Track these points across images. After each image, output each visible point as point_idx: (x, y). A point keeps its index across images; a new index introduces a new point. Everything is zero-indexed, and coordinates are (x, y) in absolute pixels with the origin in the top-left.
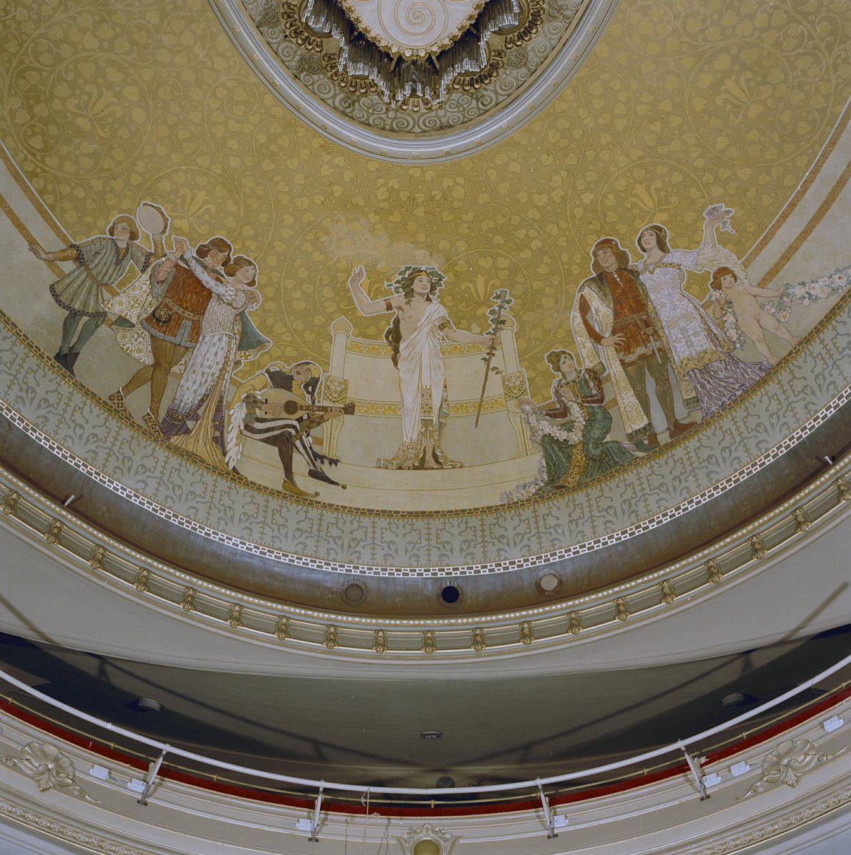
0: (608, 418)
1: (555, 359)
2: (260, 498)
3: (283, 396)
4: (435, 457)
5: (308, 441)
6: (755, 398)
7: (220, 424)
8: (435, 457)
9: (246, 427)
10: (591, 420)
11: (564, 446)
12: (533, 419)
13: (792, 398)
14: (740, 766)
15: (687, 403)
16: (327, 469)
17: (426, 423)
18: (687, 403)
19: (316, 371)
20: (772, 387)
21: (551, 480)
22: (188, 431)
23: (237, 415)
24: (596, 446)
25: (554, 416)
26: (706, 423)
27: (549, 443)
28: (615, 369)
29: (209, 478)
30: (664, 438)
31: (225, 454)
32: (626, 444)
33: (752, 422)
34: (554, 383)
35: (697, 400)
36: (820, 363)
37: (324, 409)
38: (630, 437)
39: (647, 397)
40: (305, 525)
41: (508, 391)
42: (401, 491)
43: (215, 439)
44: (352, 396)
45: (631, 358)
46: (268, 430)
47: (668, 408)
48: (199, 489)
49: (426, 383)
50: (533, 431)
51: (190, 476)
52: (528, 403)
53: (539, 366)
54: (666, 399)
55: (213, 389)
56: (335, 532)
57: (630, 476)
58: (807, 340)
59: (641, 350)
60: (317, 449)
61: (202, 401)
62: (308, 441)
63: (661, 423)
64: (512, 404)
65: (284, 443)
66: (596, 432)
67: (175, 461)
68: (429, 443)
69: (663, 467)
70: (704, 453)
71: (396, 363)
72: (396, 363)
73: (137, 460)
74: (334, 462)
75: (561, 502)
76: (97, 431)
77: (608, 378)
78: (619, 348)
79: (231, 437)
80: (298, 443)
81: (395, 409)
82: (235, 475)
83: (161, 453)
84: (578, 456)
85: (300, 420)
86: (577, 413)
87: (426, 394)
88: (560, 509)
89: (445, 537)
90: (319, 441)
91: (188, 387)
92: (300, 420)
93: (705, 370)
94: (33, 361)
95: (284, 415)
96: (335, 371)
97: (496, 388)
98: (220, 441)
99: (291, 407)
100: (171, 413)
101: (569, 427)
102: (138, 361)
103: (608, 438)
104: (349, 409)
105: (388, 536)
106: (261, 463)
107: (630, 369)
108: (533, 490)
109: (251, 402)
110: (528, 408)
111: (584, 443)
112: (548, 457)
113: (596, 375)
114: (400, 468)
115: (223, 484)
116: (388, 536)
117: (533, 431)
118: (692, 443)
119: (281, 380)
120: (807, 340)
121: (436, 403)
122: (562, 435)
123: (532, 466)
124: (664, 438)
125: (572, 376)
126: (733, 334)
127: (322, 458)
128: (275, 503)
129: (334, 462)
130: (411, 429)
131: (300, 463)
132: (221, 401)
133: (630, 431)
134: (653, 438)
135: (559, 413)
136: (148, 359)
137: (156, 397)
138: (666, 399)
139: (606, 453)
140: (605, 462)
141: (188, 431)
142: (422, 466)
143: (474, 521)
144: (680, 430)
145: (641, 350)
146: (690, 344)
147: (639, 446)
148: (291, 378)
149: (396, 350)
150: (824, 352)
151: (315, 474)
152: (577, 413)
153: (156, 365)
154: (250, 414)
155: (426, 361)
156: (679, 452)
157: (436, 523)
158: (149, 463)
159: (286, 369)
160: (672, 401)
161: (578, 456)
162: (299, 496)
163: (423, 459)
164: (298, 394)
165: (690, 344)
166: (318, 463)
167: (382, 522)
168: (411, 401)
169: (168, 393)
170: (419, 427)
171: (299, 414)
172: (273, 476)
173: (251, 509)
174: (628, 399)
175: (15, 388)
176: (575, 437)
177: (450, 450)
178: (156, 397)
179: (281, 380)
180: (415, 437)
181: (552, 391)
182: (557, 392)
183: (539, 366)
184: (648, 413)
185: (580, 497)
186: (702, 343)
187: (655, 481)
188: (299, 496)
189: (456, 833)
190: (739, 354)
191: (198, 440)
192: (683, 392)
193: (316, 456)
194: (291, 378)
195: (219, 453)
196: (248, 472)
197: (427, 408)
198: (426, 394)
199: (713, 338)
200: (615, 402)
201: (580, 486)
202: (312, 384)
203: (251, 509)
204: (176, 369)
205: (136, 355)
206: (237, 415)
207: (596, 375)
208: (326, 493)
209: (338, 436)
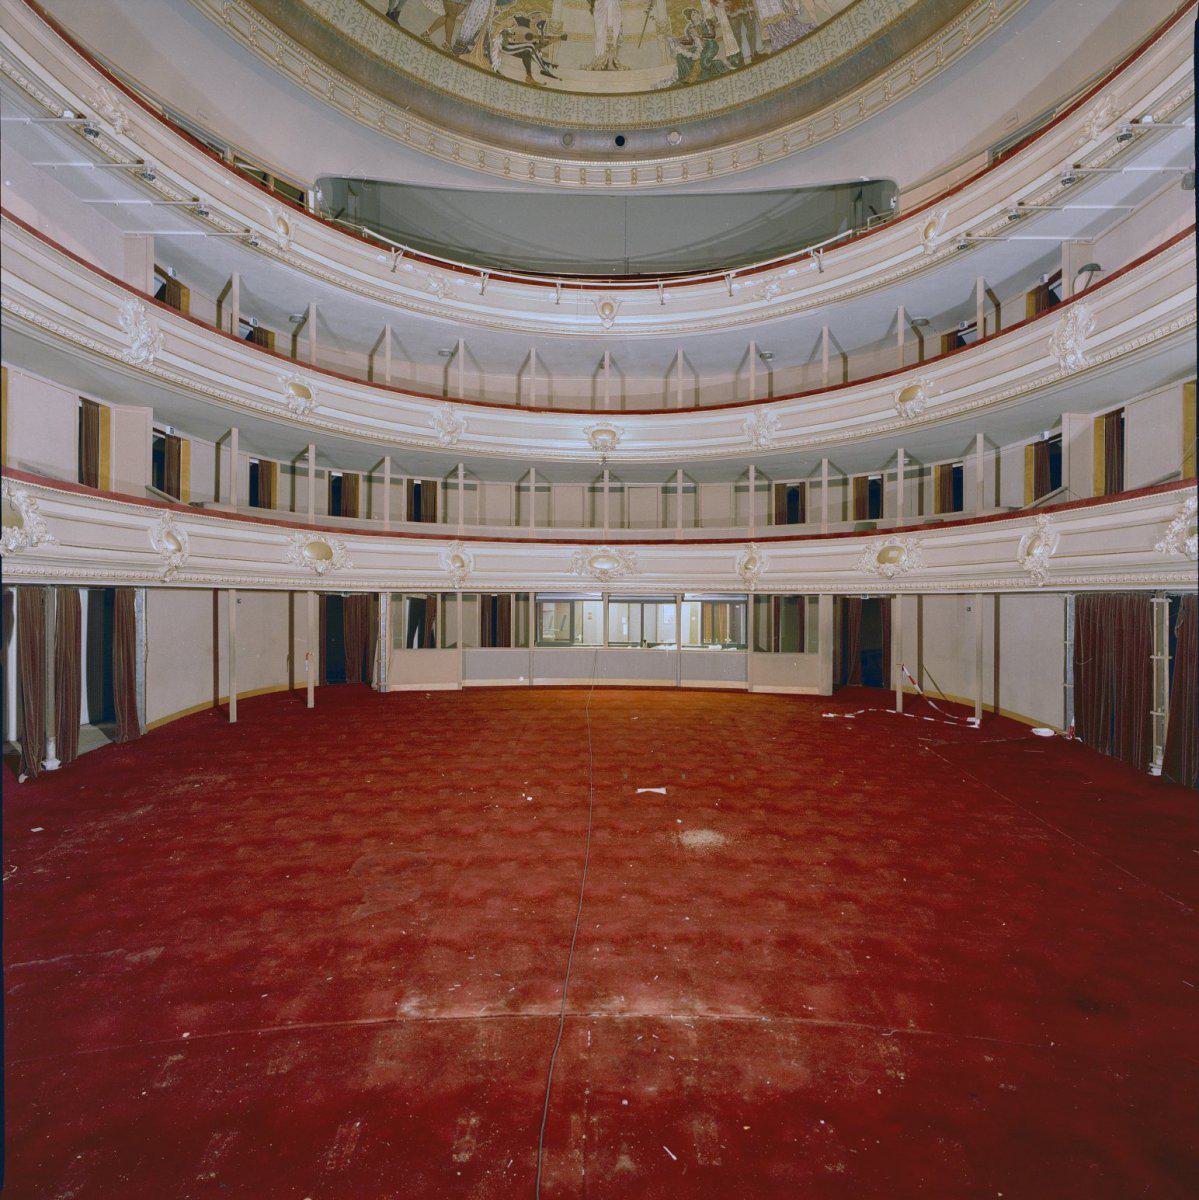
0: (716, 47)
1: (689, 13)
2: (513, 86)
3: (525, 30)
4: (614, 64)
5: (540, 55)
6: (803, 44)
7: (487, 47)
8: (614, 64)
9: (504, 48)
10: (706, 48)
11: (690, 60)
12: (673, 46)
13: (825, 47)
14: (749, 282)
15: (764, 43)
16: (550, 70)
17: (609, 46)
18: (764, 43)
19: (544, 16)
20: (814, 39)
21: (681, 79)
22: (469, 52)
23: (497, 41)
24: (709, 61)
25: (685, 44)
26: (773, 54)
27: (681, 57)
28: (724, 21)
29: (483, 76)
30: (748, 61)
31: (491, 63)
32: (725, 62)
33: (799, 58)
34: (687, 26)
35: (770, 41)
36: (845, 28)
37: (549, 37)
38: (728, 58)
39: (741, 37)
40: (539, 101)
41: (659, 30)
42: (594, 82)
43: (486, 56)
44: (565, 30)
45: (735, 15)
46: (515, 50)
47: (752, 45)
48: (478, 84)
49: (610, 24)
50: (672, 51)
51: (472, 76)
52: (669, 36)
53: (678, 16)
54: (752, 39)
55: (482, 27)
56: (556, 104)
57: (725, 80)
58: (841, 14)
59: (741, 11)
60: (545, 59)
61: (476, 35)
62: (540, 55)
63: (747, 52)
64: (661, 37)
65: (526, 57)
66: (709, 54)
67: (463, 68)
68: (610, 57)
69: (744, 75)
70: (769, 72)
71: (592, 13)
72: (592, 13)
73: (441, 70)
74: (555, 66)
75: (685, 91)
76: (416, 55)
77: (719, 25)
78: (727, 9)
79: (495, 54)
80: (534, 56)
81: (591, 38)
82: (498, 75)
83: (455, 65)
84: (697, 66)
85: (535, 44)
86: (699, 43)
87: (610, 30)
88: (684, 93)
89: (618, 107)
90: (546, 55)
91: (467, 28)
92: (535, 44)
93: (777, 25)
94: (373, 17)
95: (525, 41)
96: (555, 17)
97: (651, 27)
98: (488, 56)
99: (529, 37)
100: (459, 42)
101: (694, 50)
102: (436, 14)
103: (715, 58)
104: (564, 38)
105: (586, 106)
106: (514, 68)
107: (734, 22)
108: (669, 83)
109: (505, 34)
110: (669, 39)
111: (701, 60)
112: (680, 66)
113: (713, 23)
114: (593, 69)
115: (492, 80)
116: (586, 106)
117: (672, 51)
118: (763, 65)
119: (523, 22)
120: (841, 14)
121: (615, 35)
122: (688, 54)
123: (668, 72)
124: (748, 61)
125: (699, 23)
126: (797, 7)
127: (548, 64)
128: (522, 89)
129: (555, 66)
130: (600, 49)
131: (535, 66)
132: (487, 34)
133: (728, 55)
134: (742, 60)
135: (688, 43)
136: (442, 12)
137: (449, 33)
138: (752, 39)
139: (714, 66)
140: (713, 71)
141: (469, 52)
142: (606, 68)
143: (635, 98)
144: (758, 58)
145: (741, 11)
146: (770, 9)
147: (733, 64)
148: (529, 21)
149: (593, 6)
150: (848, 22)
151: (543, 73)
152: (699, 43)
153: (447, 15)
154: (504, 41)
155: (610, 14)
156: (755, 69)
157: (613, 100)
158: (448, 71)
159: (526, 16)
160: (755, 40)
161: (697, 66)
162: (535, 86)
163: (607, 66)
164: (533, 29)
165: (770, 9)
166: (546, 67)
167: (583, 99)
168: (601, 34)
169: (456, 30)
170: (605, 48)
171: (534, 40)
172: (520, 74)
173: (508, 93)
174: (729, 37)
175: (366, 35)
176: (696, 56)
177: (622, 61)
178: (449, 33)
179: (523, 22)
180: (603, 52)
181: (685, 30)
182: (688, 31)
183: (678, 16)
184: (740, 46)
185: (696, 89)
186: (777, 9)
187: (739, 84)
188: (535, 86)
189: (622, 298)
190: (800, 18)
191: (476, 56)
192: (762, 36)
193: (545, 63)
194: (529, 21)
195: (488, 63)
196: (505, 73)
197: (610, 38)
198: (610, 30)
199: (785, 8)
200: (721, 38)
201: (697, 83)
202: (542, 24)
203: (508, 93)
204: (459, 17)
205: (435, 11)
206: (497, 41)
207: (713, 23)
208: (551, 83)
209: (556, 52)
